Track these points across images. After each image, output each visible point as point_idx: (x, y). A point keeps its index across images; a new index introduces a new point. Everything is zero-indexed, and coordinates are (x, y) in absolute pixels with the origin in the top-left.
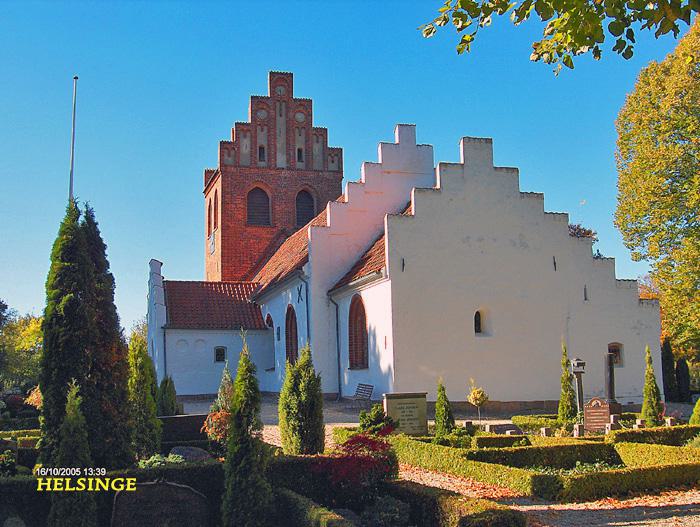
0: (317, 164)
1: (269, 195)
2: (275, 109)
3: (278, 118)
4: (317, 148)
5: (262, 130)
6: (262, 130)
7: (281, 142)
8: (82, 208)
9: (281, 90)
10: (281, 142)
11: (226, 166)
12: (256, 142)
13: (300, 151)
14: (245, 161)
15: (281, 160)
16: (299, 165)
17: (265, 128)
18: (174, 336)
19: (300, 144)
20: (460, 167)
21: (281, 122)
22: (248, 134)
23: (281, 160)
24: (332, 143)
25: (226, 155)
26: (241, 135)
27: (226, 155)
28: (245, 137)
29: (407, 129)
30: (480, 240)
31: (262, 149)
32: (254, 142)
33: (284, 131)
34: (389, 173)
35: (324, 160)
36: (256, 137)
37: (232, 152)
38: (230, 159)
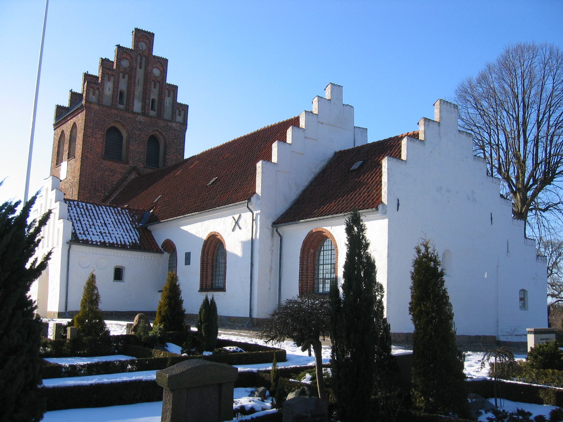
0: (167, 114)
1: (125, 135)
2: (136, 61)
3: (138, 69)
4: (168, 101)
5: (124, 77)
6: (124, 77)
7: (138, 91)
8: (554, 49)
9: (143, 46)
10: (138, 91)
11: (90, 103)
12: (118, 86)
13: (153, 101)
14: (107, 101)
15: (137, 106)
16: (153, 113)
17: (127, 76)
18: (76, 248)
19: (154, 95)
20: (436, 126)
21: (140, 73)
22: (112, 78)
23: (137, 106)
24: (180, 100)
25: (91, 94)
26: (106, 78)
27: (91, 94)
28: (109, 80)
29: (336, 88)
30: (448, 191)
31: (121, 94)
32: (116, 85)
33: (141, 82)
34: (322, 123)
35: (173, 113)
36: (118, 83)
37: (97, 92)
38: (94, 97)
